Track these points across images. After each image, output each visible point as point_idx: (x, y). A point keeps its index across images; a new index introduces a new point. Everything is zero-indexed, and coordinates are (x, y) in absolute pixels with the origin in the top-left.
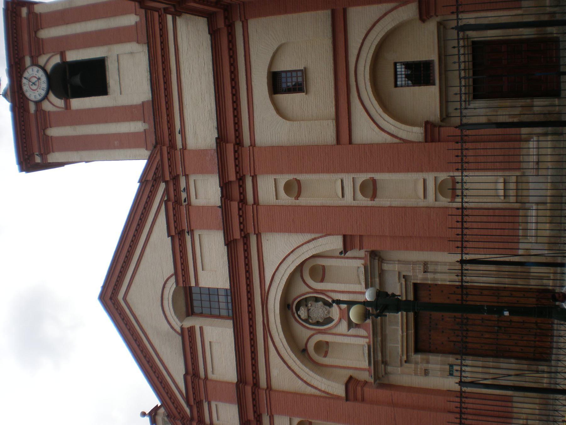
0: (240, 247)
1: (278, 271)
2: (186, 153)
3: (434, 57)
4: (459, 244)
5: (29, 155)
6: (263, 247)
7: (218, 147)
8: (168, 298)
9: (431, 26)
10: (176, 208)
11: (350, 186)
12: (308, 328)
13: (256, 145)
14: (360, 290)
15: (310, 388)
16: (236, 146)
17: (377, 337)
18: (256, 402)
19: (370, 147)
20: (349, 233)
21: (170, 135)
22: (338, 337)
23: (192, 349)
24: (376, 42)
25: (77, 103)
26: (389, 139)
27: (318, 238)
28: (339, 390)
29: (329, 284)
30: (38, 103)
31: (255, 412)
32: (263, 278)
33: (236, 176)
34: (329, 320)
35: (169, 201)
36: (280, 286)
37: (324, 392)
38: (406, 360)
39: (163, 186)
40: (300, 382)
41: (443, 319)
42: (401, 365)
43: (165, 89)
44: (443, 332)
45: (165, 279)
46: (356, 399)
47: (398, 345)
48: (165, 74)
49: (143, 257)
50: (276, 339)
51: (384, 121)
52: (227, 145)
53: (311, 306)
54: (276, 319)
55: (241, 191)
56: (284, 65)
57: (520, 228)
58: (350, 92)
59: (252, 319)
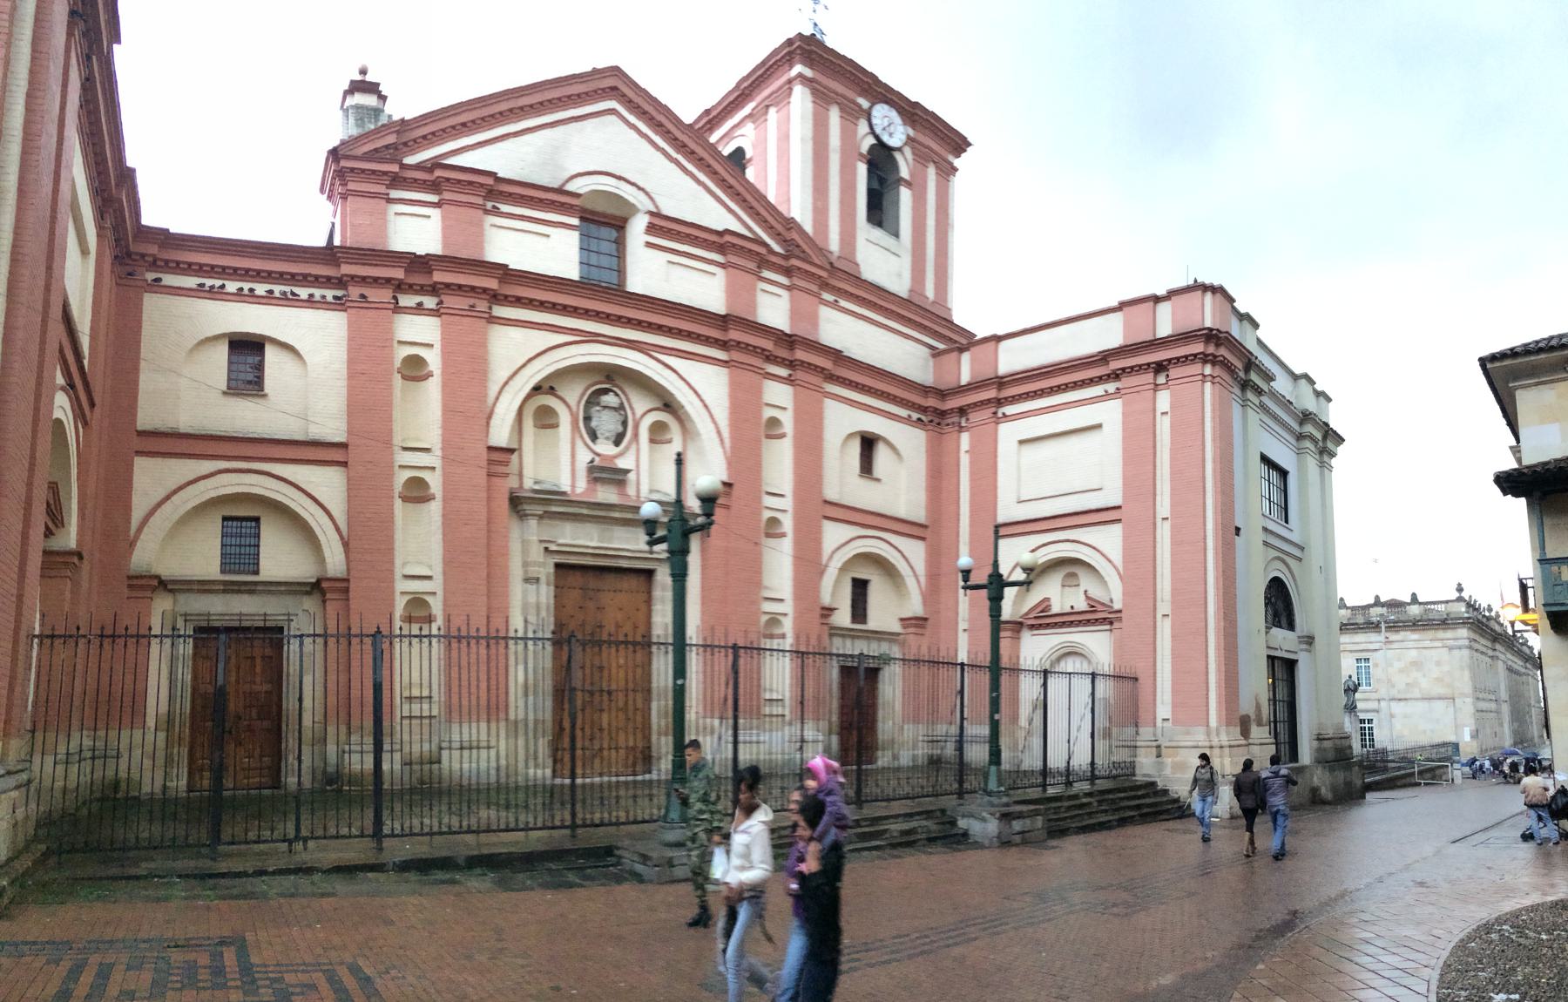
0: (714, 333)
9: (896, 627)
12: (579, 402)
22: (568, 446)
24: (293, 505)
25: (862, 169)
27: (723, 447)
28: (500, 434)
30: (868, 116)
31: (448, 286)
34: (594, 436)
39: (777, 248)
42: (541, 541)
45: (653, 195)
46: (490, 462)
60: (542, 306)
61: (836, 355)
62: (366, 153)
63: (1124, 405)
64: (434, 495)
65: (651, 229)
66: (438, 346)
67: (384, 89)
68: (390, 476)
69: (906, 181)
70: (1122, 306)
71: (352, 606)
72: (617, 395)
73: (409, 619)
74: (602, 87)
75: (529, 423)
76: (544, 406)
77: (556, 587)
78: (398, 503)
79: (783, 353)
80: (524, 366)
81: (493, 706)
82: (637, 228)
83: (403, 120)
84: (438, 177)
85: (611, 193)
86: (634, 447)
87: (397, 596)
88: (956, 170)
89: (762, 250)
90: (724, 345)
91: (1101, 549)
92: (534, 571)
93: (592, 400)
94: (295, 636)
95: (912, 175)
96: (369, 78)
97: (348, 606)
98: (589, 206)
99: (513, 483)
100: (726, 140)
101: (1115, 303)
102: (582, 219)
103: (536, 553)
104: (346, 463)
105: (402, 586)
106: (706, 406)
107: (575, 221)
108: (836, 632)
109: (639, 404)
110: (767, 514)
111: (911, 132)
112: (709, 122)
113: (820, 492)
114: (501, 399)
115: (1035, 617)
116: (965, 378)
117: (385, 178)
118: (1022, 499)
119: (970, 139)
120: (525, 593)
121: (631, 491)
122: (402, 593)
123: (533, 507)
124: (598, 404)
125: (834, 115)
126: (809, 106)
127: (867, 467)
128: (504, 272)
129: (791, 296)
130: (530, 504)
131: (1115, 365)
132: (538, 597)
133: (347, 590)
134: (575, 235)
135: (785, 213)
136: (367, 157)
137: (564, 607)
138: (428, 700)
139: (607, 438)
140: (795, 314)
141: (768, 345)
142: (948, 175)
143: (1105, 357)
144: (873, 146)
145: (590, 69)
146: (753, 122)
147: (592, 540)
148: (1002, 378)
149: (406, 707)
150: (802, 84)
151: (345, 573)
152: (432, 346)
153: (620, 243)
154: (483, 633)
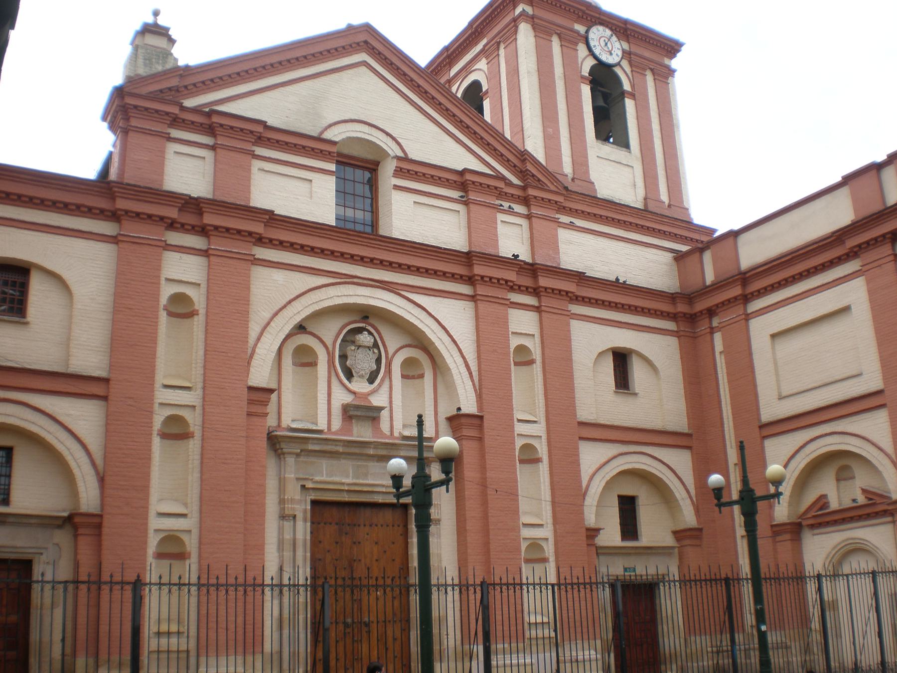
0: (527, 281)
1: (428, 315)
4: (165, 580)
6: (456, 301)
7: (576, 273)
8: (371, 135)
11: (532, 431)
13: (253, 266)
14: (395, 427)
17: (344, 446)
23: (310, 149)
26: (584, 484)
27: (473, 381)
31: (216, 228)
32: (42, 230)
34: (349, 375)
36: (408, 314)
38: (306, 487)
39: (515, 181)
41: (355, 543)
42: (298, 479)
44: (337, 543)
45: (399, 140)
46: (251, 402)
47: (325, 476)
49: (424, 117)
50: (332, 291)
52: (515, 273)
54: (362, 297)
55: (295, 246)
58: (623, 444)
59: (362, 260)
60: (303, 249)
61: (580, 277)
62: (151, 93)
63: (868, 282)
68: (150, 413)
69: (628, 93)
70: (847, 180)
72: (370, 333)
73: (160, 556)
77: (312, 523)
78: (156, 441)
80: (285, 306)
81: (249, 640)
82: (388, 170)
85: (368, 141)
86: (387, 382)
89: (501, 184)
91: (870, 438)
93: (348, 338)
96: (161, 21)
98: (346, 151)
99: (271, 421)
100: (464, 74)
101: (838, 179)
102: (338, 163)
103: (293, 491)
105: (155, 523)
107: (332, 167)
108: (601, 551)
109: (392, 341)
110: (519, 443)
111: (626, 46)
112: (448, 57)
114: (263, 339)
115: (814, 517)
116: (710, 277)
118: (784, 394)
119: (682, 40)
121: (385, 426)
122: (156, 531)
124: (353, 342)
126: (532, 40)
127: (623, 381)
128: (270, 218)
131: (852, 242)
133: (99, 526)
134: (333, 179)
135: (520, 147)
136: (150, 97)
137: (320, 542)
142: (667, 78)
143: (839, 236)
146: (487, 58)
147: (347, 476)
148: (745, 273)
151: (99, 509)
153: (373, 184)
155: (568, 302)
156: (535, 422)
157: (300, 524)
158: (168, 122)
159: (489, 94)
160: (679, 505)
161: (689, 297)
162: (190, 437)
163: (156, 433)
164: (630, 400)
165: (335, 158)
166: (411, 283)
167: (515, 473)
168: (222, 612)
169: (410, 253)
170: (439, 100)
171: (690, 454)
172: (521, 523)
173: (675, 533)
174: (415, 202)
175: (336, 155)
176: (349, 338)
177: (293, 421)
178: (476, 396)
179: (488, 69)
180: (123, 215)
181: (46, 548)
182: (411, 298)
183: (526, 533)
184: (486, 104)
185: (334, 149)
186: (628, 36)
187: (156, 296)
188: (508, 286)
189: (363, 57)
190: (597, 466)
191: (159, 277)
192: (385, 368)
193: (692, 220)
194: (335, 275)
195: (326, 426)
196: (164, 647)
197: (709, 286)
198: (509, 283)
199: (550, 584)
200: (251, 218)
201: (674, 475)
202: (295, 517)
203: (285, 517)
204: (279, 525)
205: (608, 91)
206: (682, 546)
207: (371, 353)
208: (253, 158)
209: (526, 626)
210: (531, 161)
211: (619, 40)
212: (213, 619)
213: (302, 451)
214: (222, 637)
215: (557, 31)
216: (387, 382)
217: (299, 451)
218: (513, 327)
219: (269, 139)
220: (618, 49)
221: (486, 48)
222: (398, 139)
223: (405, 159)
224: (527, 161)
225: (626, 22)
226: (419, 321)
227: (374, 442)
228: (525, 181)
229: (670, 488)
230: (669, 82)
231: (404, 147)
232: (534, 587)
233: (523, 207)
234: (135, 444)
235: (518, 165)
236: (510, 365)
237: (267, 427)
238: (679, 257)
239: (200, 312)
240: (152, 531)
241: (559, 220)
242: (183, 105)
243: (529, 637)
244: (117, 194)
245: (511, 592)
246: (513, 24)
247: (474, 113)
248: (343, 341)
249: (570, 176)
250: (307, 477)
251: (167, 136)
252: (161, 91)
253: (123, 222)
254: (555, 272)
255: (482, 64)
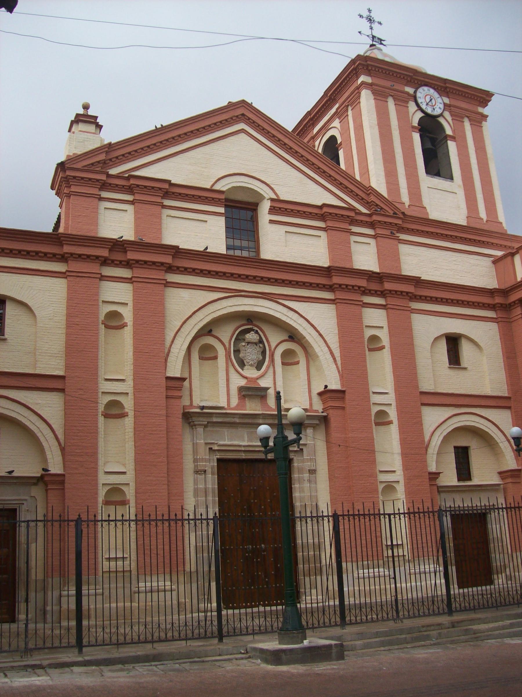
2: (349, 234)
3: (476, 481)
5: (371, 71)
9: (496, 480)
10: (348, 219)
11: (385, 400)
15: (172, 335)
16: (103, 259)
17: (239, 418)
18: (150, 265)
19: (419, 423)
20: (347, 396)
21: (408, 229)
25: (416, 137)
26: (427, 439)
27: (336, 364)
29: (281, 369)
31: (137, 261)
33: (67, 253)
34: (242, 364)
35: (107, 177)
37: (169, 351)
38: (213, 449)
39: (364, 210)
40: (180, 324)
42: (206, 444)
43: (442, 234)
45: (272, 186)
46: (168, 388)
48: (182, 195)
51: (438, 436)
52: (365, 281)
53: (260, 346)
54: (248, 306)
56: (466, 349)
57: (369, 562)
59: (247, 278)
60: (202, 273)
61: (417, 281)
64: (127, 413)
65: (273, 210)
66: (131, 304)
67: (100, 121)
69: (450, 136)
71: (66, 495)
72: (257, 332)
73: (107, 503)
74: (236, 115)
75: (195, 356)
76: (206, 344)
78: (101, 419)
79: (374, 286)
80: (190, 317)
82: (265, 207)
83: (110, 144)
84: (132, 184)
86: (271, 370)
87: (100, 486)
88: (487, 116)
89: (352, 214)
90: (330, 288)
92: (201, 465)
94: (24, 522)
95: (454, 131)
96: (91, 112)
97: (64, 493)
98: (232, 197)
100: (323, 131)
102: (226, 206)
103: (203, 453)
104: (64, 390)
105: (103, 479)
106: (321, 335)
107: (222, 210)
110: (375, 409)
111: (447, 100)
113: (417, 387)
117: (97, 183)
120: (196, 482)
123: (201, 419)
125: (391, 104)
126: (372, 102)
129: (377, 243)
130: (198, 417)
132: (205, 484)
133: (63, 483)
134: (223, 219)
138: (122, 560)
139: (251, 365)
140: (381, 256)
141: (363, 283)
142: (481, 123)
144: (421, 119)
145: (225, 104)
146: (339, 118)
147: (244, 441)
149: (106, 563)
150: (367, 88)
152: (127, 304)
153: (254, 221)
154: (166, 517)
155: (408, 300)
156: (386, 393)
157: (209, 476)
158: (99, 187)
159: (342, 146)
160: (502, 452)
161: (504, 292)
162: (125, 416)
163: (100, 413)
164: (461, 373)
165: (224, 203)
166: (285, 293)
167: (372, 433)
168: (154, 542)
169: (283, 270)
170: (301, 153)
171: (510, 412)
172: (378, 470)
173: (500, 473)
174: (286, 232)
175: (224, 201)
176: (240, 337)
177: (201, 401)
178: (339, 376)
179: (340, 126)
180: (69, 257)
181: (26, 500)
182: (287, 304)
183: (382, 477)
184: (341, 153)
185: (223, 197)
186: (369, 71)
187: (96, 315)
188: (361, 291)
189: (242, 126)
190: (437, 425)
191: (98, 300)
192: (269, 358)
193: (506, 231)
194: (228, 291)
195: (226, 403)
196: (113, 569)
197: (519, 282)
198: (410, 295)
199: (387, 514)
200: (162, 252)
201: (497, 430)
202: (205, 471)
203: (199, 471)
204: (194, 478)
205: (435, 137)
206: (505, 483)
207: (258, 347)
208: (162, 208)
209: (385, 548)
210: (375, 194)
211: (441, 96)
212: (147, 547)
213: (208, 422)
214: (154, 561)
215: (391, 94)
216: (271, 370)
217: (206, 423)
218: (367, 321)
219: (173, 193)
220: (440, 103)
221: (339, 111)
222: (271, 185)
223: (279, 201)
224: (371, 195)
225: (446, 81)
226: (293, 321)
227: (263, 414)
228: (371, 209)
229: (494, 438)
230: (482, 125)
231: (276, 191)
232: (375, 517)
233: (370, 230)
234: (86, 422)
235: (365, 198)
236: (365, 351)
237: (182, 407)
238: (496, 261)
239: (128, 324)
240: (101, 485)
241: (400, 238)
242: (109, 173)
243: (387, 556)
244: (64, 242)
245: (357, 520)
246: (357, 91)
247: (329, 162)
248: (236, 339)
249: (407, 204)
250: (213, 442)
251: (99, 197)
252: (92, 164)
253: (70, 262)
254: (398, 278)
255: (336, 123)
